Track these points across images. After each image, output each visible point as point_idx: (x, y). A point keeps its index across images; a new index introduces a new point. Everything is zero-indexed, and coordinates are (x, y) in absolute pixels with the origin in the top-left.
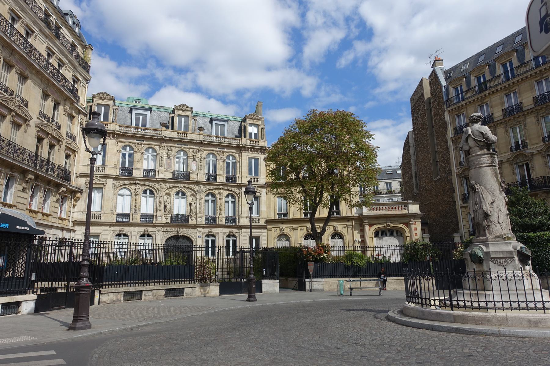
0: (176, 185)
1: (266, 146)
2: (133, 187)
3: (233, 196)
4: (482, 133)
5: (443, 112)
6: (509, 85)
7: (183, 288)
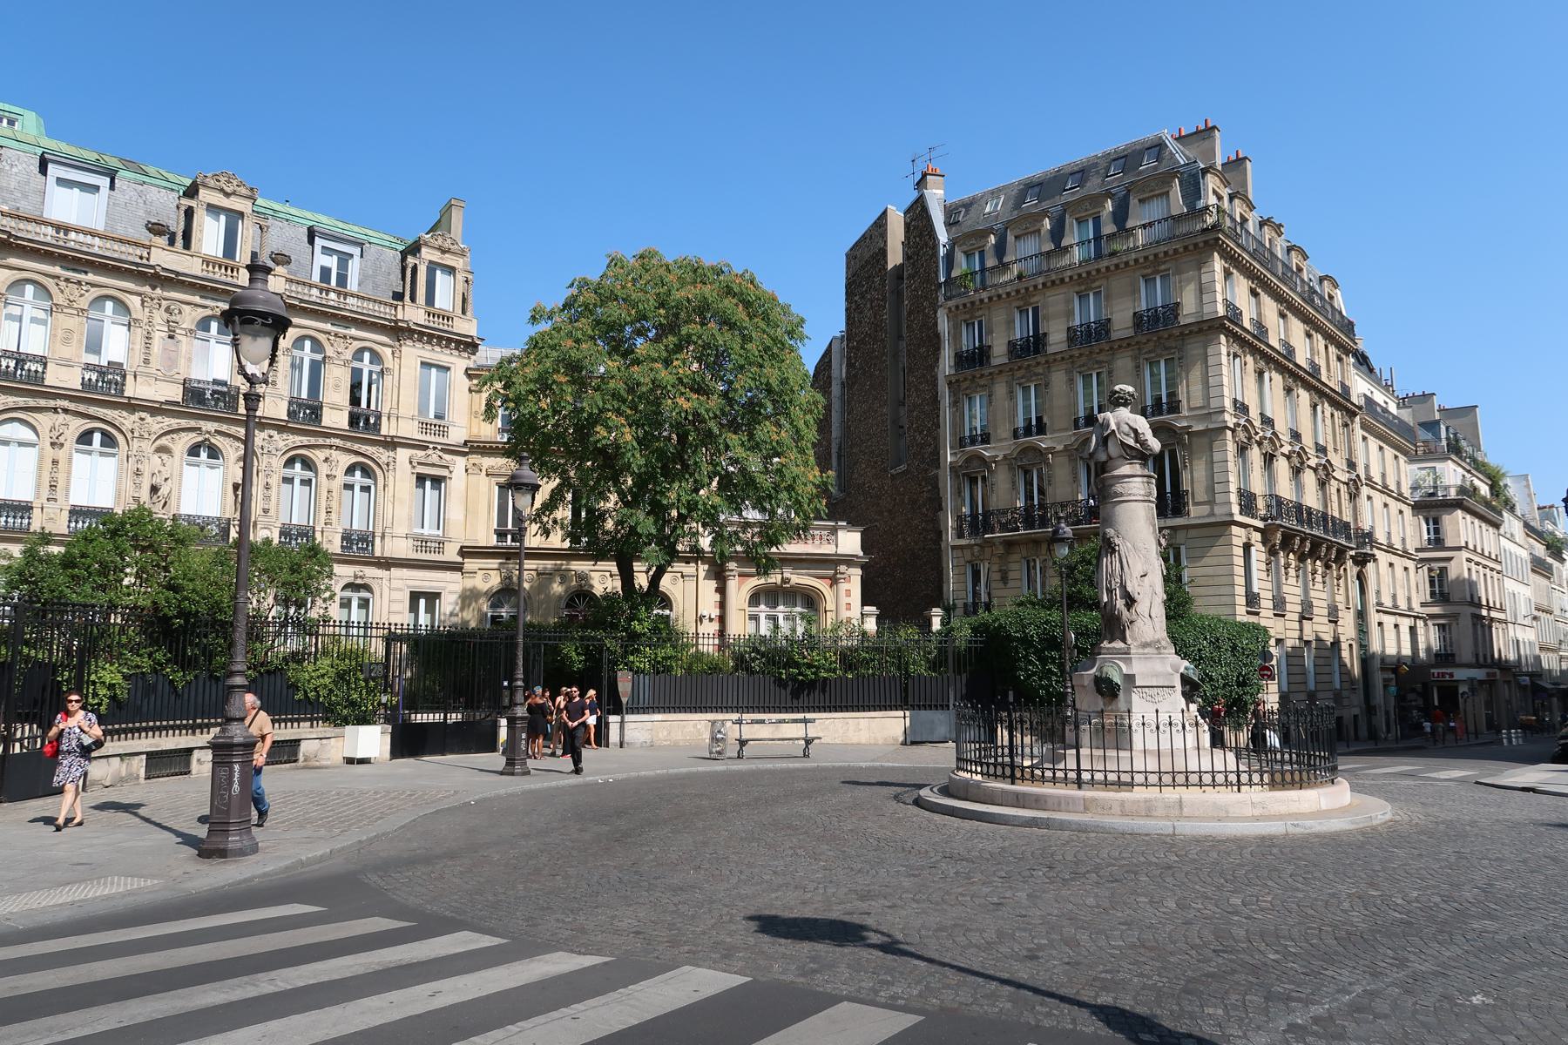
0: (193, 423)
1: (474, 333)
2: (44, 421)
3: (367, 472)
4: (1135, 431)
5: (935, 307)
6: (1089, 273)
7: (297, 742)
